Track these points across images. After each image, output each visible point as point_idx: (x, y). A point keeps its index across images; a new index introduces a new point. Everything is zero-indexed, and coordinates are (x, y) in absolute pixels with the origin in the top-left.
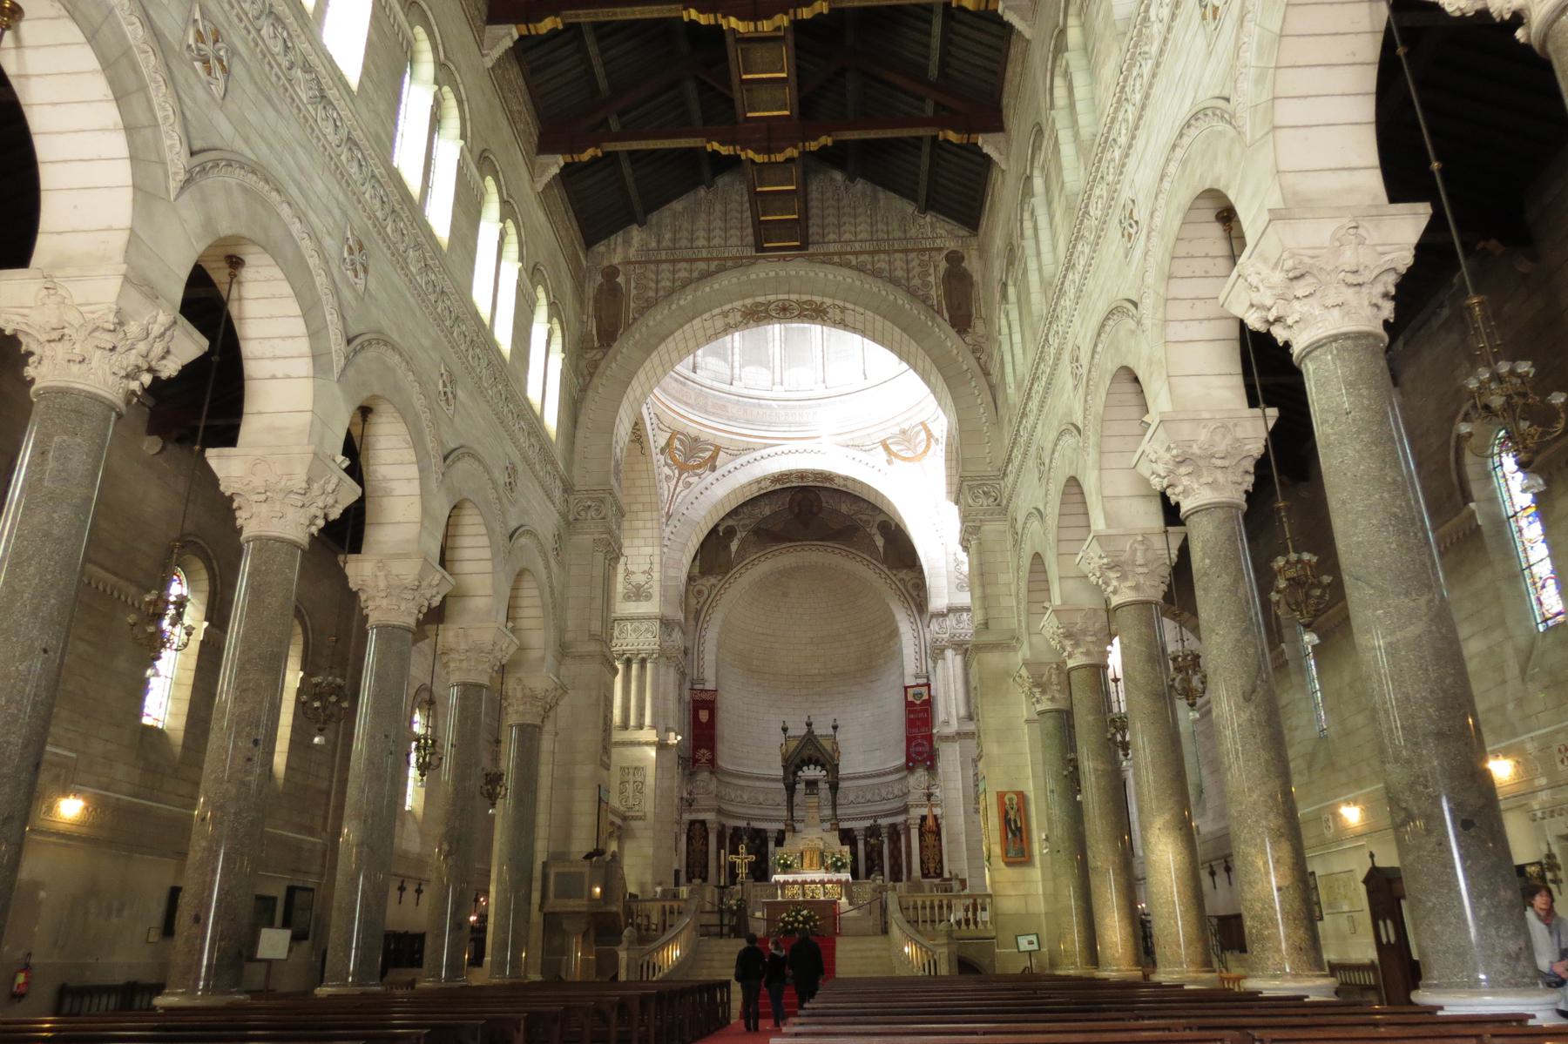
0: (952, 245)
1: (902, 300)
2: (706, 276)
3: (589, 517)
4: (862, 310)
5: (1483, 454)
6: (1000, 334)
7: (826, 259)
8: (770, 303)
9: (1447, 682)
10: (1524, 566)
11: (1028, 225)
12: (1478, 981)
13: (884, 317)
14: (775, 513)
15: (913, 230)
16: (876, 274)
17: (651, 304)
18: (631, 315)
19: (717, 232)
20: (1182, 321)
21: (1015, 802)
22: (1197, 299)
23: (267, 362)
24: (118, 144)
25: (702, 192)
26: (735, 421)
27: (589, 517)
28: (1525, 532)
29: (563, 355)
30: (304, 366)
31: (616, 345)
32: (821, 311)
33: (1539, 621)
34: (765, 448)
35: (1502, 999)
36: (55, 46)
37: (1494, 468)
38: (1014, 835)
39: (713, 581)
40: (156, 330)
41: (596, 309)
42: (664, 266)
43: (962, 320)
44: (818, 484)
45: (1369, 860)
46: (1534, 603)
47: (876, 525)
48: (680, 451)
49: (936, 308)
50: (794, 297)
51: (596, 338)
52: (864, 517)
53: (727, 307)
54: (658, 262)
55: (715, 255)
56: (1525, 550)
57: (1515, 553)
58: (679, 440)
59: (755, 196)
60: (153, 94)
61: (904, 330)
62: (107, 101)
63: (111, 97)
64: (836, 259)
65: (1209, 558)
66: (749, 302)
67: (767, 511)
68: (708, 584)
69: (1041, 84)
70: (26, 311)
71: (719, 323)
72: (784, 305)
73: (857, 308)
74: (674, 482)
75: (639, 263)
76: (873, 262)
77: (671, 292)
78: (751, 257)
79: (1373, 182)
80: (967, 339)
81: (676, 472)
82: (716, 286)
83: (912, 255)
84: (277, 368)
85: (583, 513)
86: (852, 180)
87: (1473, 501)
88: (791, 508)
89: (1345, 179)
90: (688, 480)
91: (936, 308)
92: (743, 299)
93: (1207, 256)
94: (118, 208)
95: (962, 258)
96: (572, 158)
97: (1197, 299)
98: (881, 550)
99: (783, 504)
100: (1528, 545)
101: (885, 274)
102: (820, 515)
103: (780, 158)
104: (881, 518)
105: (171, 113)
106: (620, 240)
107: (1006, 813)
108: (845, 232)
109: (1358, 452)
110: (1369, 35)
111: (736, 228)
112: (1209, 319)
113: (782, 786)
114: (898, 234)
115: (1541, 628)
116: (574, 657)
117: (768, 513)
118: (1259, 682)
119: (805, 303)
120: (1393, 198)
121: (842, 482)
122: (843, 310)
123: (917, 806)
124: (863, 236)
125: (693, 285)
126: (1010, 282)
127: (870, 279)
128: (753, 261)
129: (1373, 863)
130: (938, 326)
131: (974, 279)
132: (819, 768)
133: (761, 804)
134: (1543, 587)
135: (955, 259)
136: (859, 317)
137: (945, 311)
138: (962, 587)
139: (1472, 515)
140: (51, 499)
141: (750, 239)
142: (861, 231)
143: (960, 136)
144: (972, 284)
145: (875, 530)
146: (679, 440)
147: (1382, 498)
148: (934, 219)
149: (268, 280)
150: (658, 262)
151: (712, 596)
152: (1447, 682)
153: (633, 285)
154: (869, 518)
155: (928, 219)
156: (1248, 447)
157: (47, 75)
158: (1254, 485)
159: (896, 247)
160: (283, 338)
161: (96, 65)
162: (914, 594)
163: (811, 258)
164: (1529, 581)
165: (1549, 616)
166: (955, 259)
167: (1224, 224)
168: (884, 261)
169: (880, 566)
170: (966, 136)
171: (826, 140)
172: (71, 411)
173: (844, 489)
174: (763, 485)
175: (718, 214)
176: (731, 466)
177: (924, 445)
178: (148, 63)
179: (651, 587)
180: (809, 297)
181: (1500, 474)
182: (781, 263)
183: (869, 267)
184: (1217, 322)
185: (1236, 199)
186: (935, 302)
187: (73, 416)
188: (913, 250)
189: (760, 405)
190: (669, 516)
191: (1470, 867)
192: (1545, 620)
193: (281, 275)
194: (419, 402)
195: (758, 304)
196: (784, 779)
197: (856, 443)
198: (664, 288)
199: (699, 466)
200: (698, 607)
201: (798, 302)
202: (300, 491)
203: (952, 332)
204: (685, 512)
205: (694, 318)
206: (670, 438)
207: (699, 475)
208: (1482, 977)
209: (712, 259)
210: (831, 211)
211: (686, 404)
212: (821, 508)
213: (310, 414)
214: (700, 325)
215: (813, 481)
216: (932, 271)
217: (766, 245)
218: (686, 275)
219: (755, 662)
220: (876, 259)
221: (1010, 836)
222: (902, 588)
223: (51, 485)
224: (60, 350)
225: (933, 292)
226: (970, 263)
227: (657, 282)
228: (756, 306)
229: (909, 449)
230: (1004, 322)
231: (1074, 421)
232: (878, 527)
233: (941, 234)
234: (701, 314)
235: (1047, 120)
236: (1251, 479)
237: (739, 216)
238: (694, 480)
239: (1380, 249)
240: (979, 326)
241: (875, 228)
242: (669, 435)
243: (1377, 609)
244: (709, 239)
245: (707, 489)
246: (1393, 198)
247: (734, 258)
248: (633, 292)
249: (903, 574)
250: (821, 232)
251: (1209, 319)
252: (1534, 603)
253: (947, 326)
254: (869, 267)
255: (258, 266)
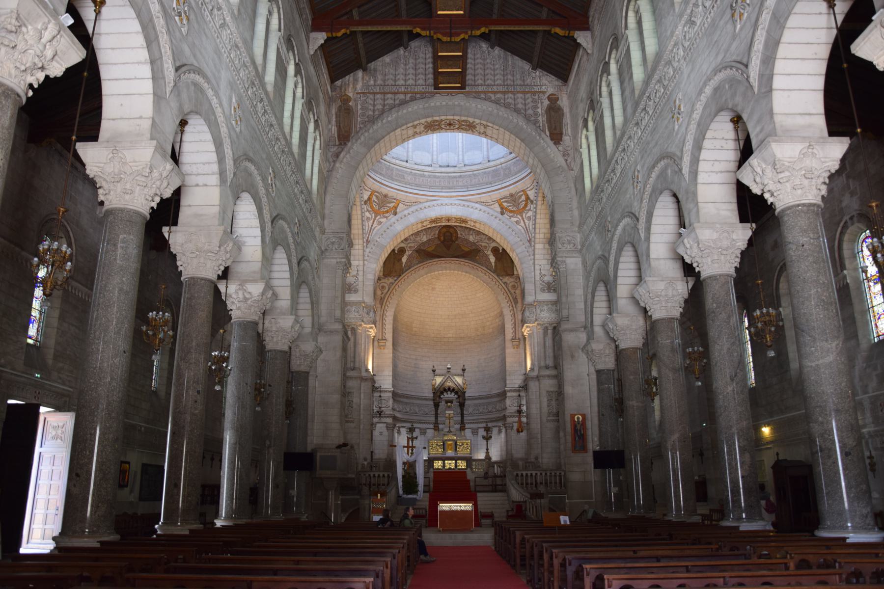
0: (550, 91)
1: (522, 122)
2: (403, 103)
3: (334, 249)
4: (497, 128)
5: (854, 239)
6: (581, 148)
7: (477, 95)
8: (442, 121)
9: (843, 385)
10: (870, 306)
11: (604, 89)
12: (848, 527)
13: (511, 133)
14: (429, 240)
15: (529, 80)
16: (507, 106)
17: (372, 120)
18: (358, 126)
19: (410, 76)
20: (707, 172)
21: (581, 419)
22: (716, 161)
23: (194, 176)
24: (146, 71)
25: (401, 51)
26: (409, 185)
27: (334, 249)
28: (872, 288)
29: (320, 151)
30: (215, 180)
31: (349, 144)
32: (472, 126)
33: (875, 336)
34: (427, 202)
35: (859, 535)
36: (118, 19)
37: (858, 253)
38: (579, 438)
39: (391, 280)
40: (165, 174)
41: (336, 121)
42: (378, 96)
43: (556, 137)
44: (458, 224)
45: (776, 457)
46: (874, 326)
47: (490, 249)
48: (376, 202)
49: (541, 128)
50: (457, 118)
51: (337, 139)
52: (483, 244)
53: (416, 123)
54: (374, 94)
55: (409, 90)
56: (871, 298)
57: (866, 299)
58: (376, 196)
59: (436, 58)
60: (160, 40)
61: (522, 140)
62: (143, 48)
63: (145, 45)
64: (483, 96)
65: (716, 303)
66: (429, 120)
67: (425, 239)
68: (388, 282)
69: (619, 12)
70: (102, 165)
71: (411, 132)
72: (450, 122)
73: (495, 126)
74: (372, 221)
75: (363, 93)
76: (505, 98)
77: (383, 112)
78: (432, 93)
79: (821, 122)
80: (560, 148)
81: (373, 215)
82: (410, 109)
83: (528, 95)
84: (200, 180)
85: (330, 246)
86: (492, 48)
87: (845, 270)
88: (439, 238)
89: (807, 120)
90: (380, 220)
91: (541, 128)
92: (427, 118)
93: (723, 139)
94: (145, 106)
95: (558, 99)
96: (332, 34)
97: (716, 161)
98: (493, 264)
99: (434, 235)
100: (873, 295)
101: (512, 106)
102: (457, 242)
103: (458, 39)
104: (493, 245)
105: (168, 49)
106: (351, 79)
107: (575, 426)
108: (488, 80)
109: (807, 266)
110: (825, 30)
111: (422, 74)
112: (721, 172)
113: (431, 403)
114: (519, 82)
115: (876, 340)
116: (326, 332)
117: (426, 240)
118: (738, 371)
119: (463, 121)
120: (832, 133)
121: (472, 224)
122: (485, 127)
123: (511, 416)
124: (499, 82)
125: (396, 109)
126: (590, 119)
127: (503, 109)
128: (432, 95)
129: (778, 458)
130: (543, 139)
131: (565, 111)
132: (453, 394)
133: (427, 414)
134: (879, 318)
135: (553, 99)
136: (495, 131)
137: (547, 130)
138: (544, 290)
139: (845, 277)
140: (121, 270)
141: (431, 81)
142: (498, 79)
143: (563, 32)
144: (563, 114)
145: (489, 252)
146: (376, 196)
147: (817, 291)
148: (541, 74)
149: (199, 132)
150: (374, 94)
151: (391, 289)
152: (843, 385)
153: (359, 107)
154: (487, 245)
155: (538, 73)
156: (738, 244)
157: (111, 33)
158: (740, 263)
159: (518, 90)
160: (204, 164)
161: (139, 29)
162: (512, 291)
163: (468, 94)
164: (871, 315)
165: (881, 334)
166: (553, 99)
167: (734, 124)
168: (511, 98)
169: (492, 274)
170: (567, 32)
171: (483, 30)
172: (127, 221)
173: (474, 228)
174: (425, 224)
175: (411, 65)
176: (406, 212)
177: (523, 203)
178: (159, 23)
179: (358, 285)
180: (466, 118)
181: (861, 256)
182: (449, 97)
183: (502, 101)
184: (726, 173)
185: (748, 120)
186: (541, 125)
187: (128, 223)
188: (528, 93)
189: (424, 176)
190: (368, 242)
191: (848, 474)
192: (878, 336)
193: (208, 130)
194: (262, 191)
195: (434, 121)
196: (434, 400)
197: (482, 200)
198: (378, 109)
199: (387, 212)
200: (382, 296)
201: (458, 121)
202: (215, 252)
203: (551, 143)
204: (378, 240)
205: (396, 129)
206: (370, 195)
207: (387, 217)
208: (849, 525)
209: (408, 93)
210: (480, 66)
211: (381, 174)
212: (457, 238)
213: (218, 207)
214: (400, 132)
215: (455, 222)
216: (539, 105)
217: (440, 85)
218: (392, 102)
219: (414, 329)
220: (506, 97)
221: (577, 438)
222: (505, 288)
223: (121, 263)
224: (119, 187)
225: (540, 119)
226: (562, 101)
227: (374, 105)
228: (434, 122)
229: (514, 206)
230: (584, 141)
231: (633, 211)
232: (492, 250)
233: (547, 84)
234: (401, 127)
235: (623, 36)
236: (738, 260)
237: (424, 66)
238: (384, 220)
239: (823, 160)
240: (567, 139)
241: (506, 78)
242: (370, 193)
243: (811, 347)
244: (406, 80)
245: (391, 226)
246: (832, 133)
247: (420, 93)
248: (360, 112)
249: (506, 279)
250: (473, 78)
251: (721, 172)
252: (874, 326)
253: (548, 140)
254: (502, 101)
255: (194, 125)
